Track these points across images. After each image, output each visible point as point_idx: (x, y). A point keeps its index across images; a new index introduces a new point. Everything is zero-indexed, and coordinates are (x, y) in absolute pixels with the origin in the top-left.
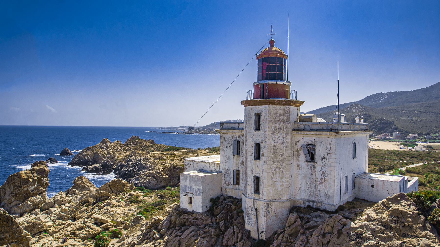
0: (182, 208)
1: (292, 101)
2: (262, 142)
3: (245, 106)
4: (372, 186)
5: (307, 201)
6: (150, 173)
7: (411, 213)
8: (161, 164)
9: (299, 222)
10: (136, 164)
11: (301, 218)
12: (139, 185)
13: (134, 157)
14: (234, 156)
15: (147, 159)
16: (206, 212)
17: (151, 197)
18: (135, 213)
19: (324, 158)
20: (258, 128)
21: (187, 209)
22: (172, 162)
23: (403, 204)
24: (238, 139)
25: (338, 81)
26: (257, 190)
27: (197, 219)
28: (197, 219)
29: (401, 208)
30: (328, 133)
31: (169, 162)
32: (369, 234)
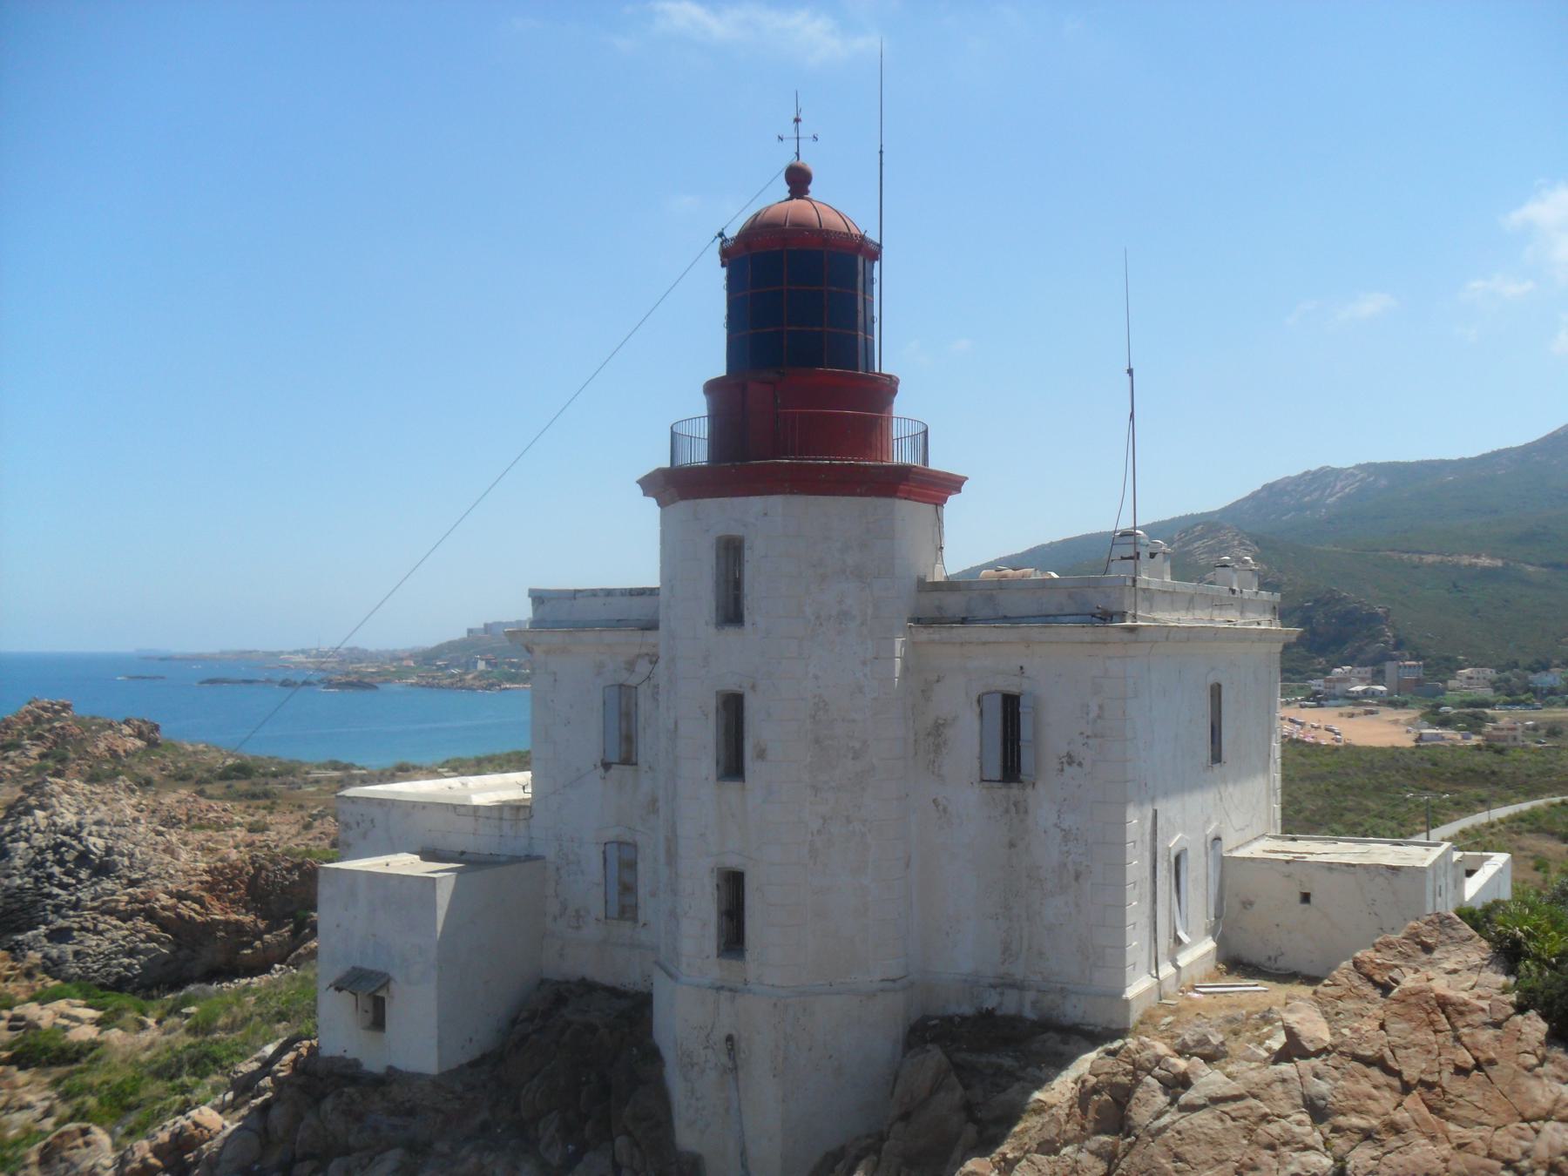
0: (331, 1059)
1: (904, 472)
2: (753, 687)
3: (661, 504)
4: (1306, 898)
5: (993, 986)
6: (133, 899)
7: (1484, 1004)
8: (202, 848)
9: (955, 1095)
10: (56, 848)
11: (958, 1067)
12: (73, 969)
13: (39, 813)
14: (606, 766)
15: (120, 824)
16: (460, 1069)
17: (143, 1026)
18: (48, 1124)
19: (1070, 759)
20: (732, 613)
21: (356, 1063)
22: (257, 837)
23: (1449, 966)
24: (624, 677)
25: (1130, 372)
26: (733, 939)
27: (411, 1112)
28: (411, 1112)
29: (1441, 985)
30: (1087, 633)
31: (240, 834)
32: (1300, 1123)
